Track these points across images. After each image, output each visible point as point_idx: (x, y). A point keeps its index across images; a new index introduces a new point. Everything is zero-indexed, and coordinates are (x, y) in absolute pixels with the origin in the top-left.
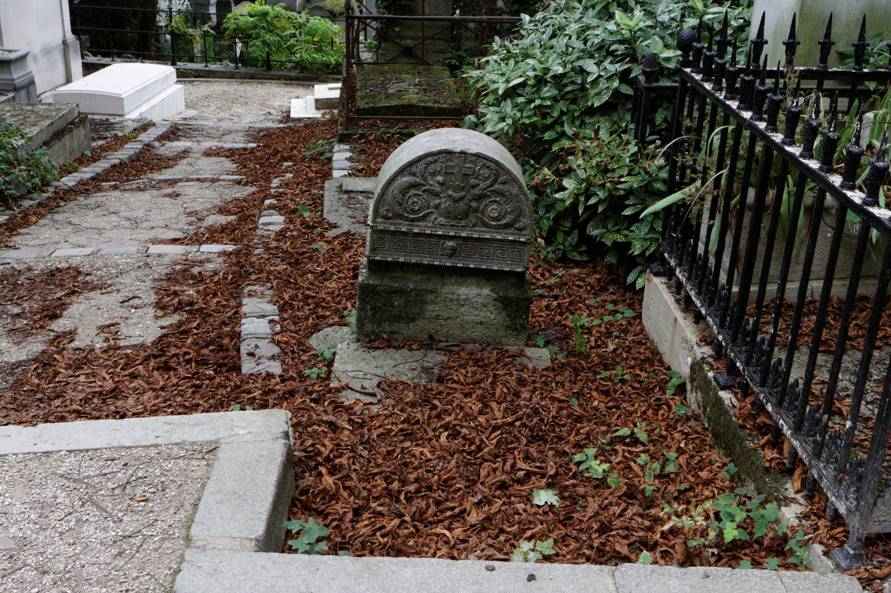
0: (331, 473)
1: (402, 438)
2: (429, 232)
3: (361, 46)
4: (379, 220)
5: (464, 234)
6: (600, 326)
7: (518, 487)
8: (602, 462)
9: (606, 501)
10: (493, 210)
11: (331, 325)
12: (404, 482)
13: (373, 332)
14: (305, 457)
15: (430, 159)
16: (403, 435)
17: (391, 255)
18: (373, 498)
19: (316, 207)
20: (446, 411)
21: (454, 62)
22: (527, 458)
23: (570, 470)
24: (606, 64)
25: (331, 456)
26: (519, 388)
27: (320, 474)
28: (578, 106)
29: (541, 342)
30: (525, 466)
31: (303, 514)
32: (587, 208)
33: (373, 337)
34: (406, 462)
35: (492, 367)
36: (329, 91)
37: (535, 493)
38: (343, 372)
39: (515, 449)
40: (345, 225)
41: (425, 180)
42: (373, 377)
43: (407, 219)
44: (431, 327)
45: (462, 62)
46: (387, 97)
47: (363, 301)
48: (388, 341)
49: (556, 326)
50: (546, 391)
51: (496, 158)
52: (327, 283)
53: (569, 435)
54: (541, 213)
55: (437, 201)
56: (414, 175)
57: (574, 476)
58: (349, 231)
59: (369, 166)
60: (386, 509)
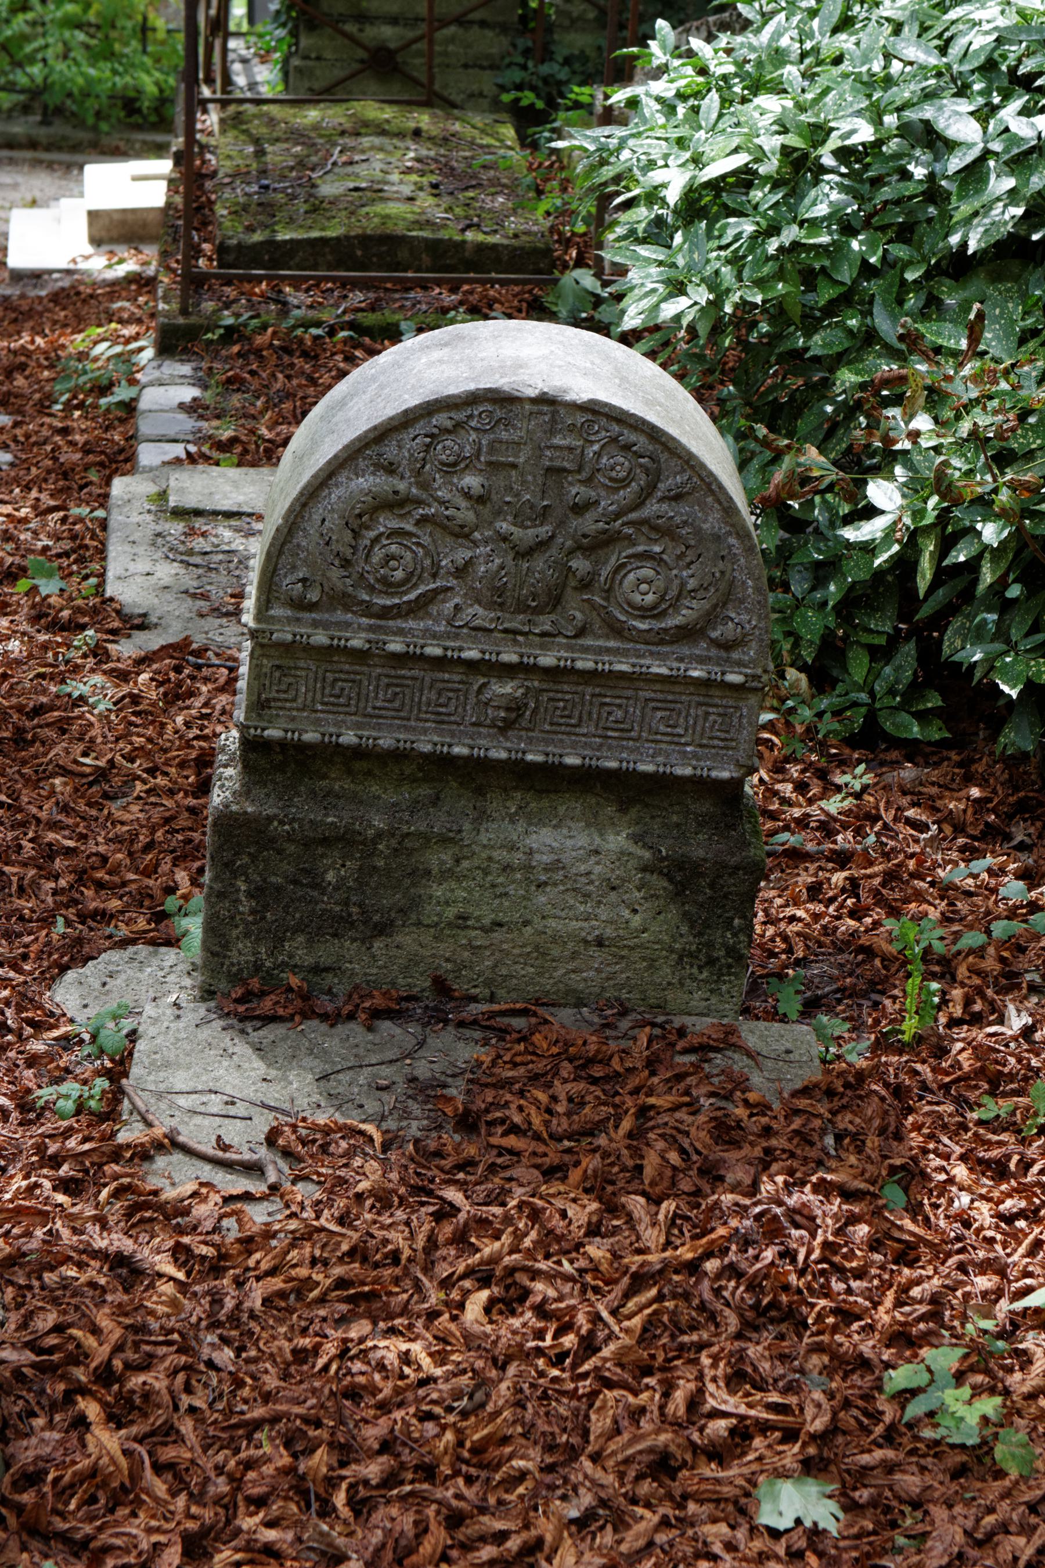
0: (115, 1420)
1: (344, 1307)
2: (438, 652)
3: (232, 44)
4: (277, 611)
5: (547, 660)
6: (980, 952)
7: (710, 1470)
8: (977, 1391)
9: (990, 1520)
10: (640, 585)
11: (124, 943)
12: (346, 1453)
13: (257, 967)
14: (33, 1365)
15: (441, 419)
16: (348, 1300)
17: (317, 722)
18: (250, 1500)
19: (81, 561)
20: (483, 1223)
21: (528, 98)
22: (739, 1378)
23: (876, 1416)
24: (1009, 114)
25: (118, 1364)
26: (718, 1153)
27: (81, 1423)
28: (919, 248)
29: (792, 1005)
30: (733, 1403)
31: (24, 1548)
32: (943, 574)
33: (255, 984)
34: (354, 1385)
35: (633, 1082)
36: (134, 183)
37: (762, 1491)
38: (160, 1095)
39: (701, 1346)
40: (176, 622)
41: (425, 486)
42: (254, 1111)
43: (367, 610)
44: (441, 953)
45: (553, 95)
46: (315, 210)
47: (227, 868)
48: (305, 997)
49: (841, 951)
50: (805, 1160)
51: (652, 417)
52: (114, 808)
53: (876, 1305)
54: (798, 588)
55: (462, 555)
56: (390, 469)
57: (890, 1437)
58: (187, 642)
59: (253, 432)
60: (289, 1536)
